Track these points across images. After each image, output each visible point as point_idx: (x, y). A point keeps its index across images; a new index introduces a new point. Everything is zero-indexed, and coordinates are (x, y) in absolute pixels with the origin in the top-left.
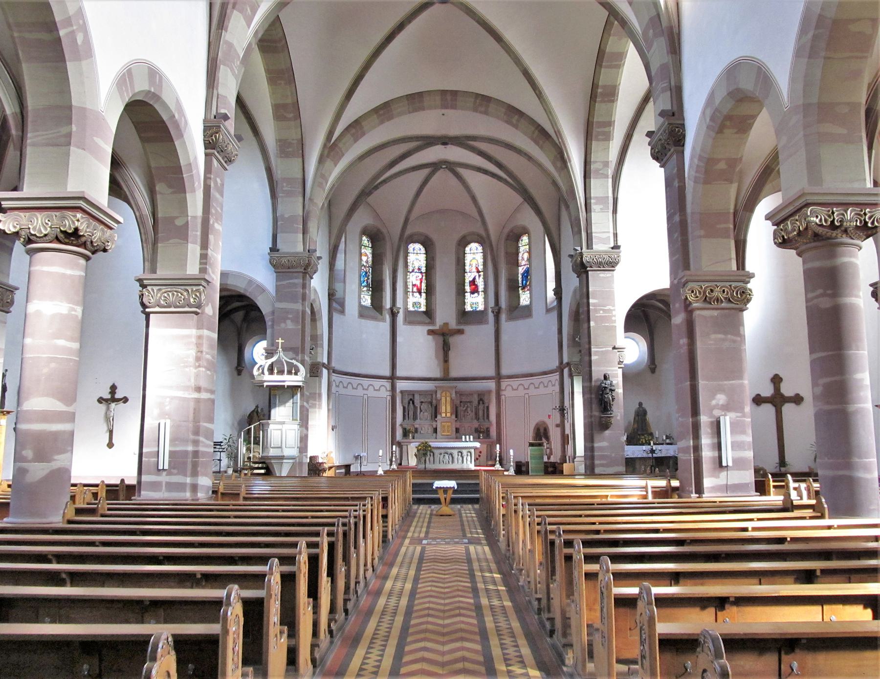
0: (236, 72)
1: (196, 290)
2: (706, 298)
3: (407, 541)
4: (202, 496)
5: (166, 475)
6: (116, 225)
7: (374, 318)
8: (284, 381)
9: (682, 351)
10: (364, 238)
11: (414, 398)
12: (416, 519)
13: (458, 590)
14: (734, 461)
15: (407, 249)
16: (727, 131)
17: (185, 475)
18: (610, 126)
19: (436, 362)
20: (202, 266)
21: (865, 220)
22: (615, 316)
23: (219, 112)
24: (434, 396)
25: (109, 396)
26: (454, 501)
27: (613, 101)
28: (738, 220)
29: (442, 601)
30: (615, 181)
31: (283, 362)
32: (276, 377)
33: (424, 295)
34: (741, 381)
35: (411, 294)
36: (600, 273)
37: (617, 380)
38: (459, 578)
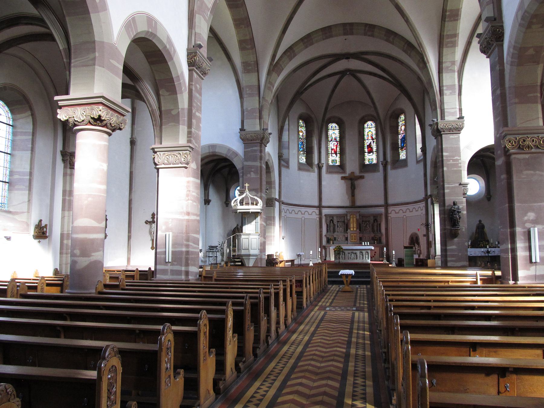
1: (185, 153)
2: (519, 146)
3: (317, 308)
5: (171, 265)
6: (127, 114)
7: (308, 171)
8: (249, 209)
9: (503, 183)
10: (301, 121)
11: (333, 218)
12: (327, 294)
15: (328, 127)
16: (534, 27)
17: (181, 266)
18: (456, 37)
19: (347, 197)
22: (461, 163)
24: (346, 217)
25: (151, 220)
26: (352, 283)
27: (457, 20)
30: (460, 75)
31: (248, 198)
32: (244, 207)
33: (338, 155)
36: (450, 136)
37: (463, 205)
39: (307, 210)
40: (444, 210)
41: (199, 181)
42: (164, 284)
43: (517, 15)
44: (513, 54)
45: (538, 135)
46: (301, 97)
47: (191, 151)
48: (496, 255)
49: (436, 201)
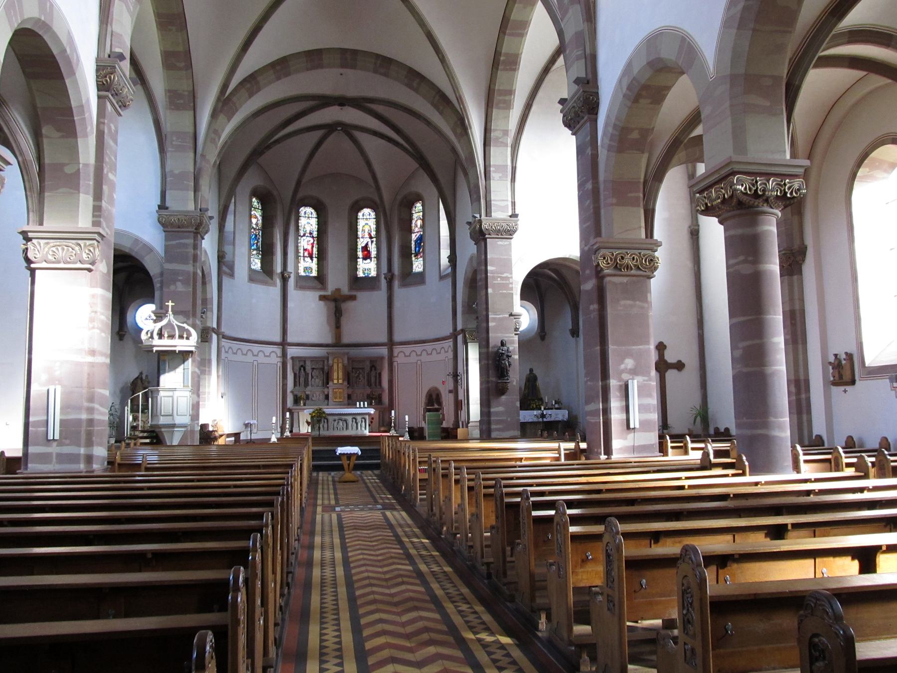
0: (132, 10)
1: (90, 245)
2: (616, 265)
3: (319, 509)
4: (98, 467)
5: (57, 446)
7: (265, 283)
8: (175, 346)
9: (592, 317)
10: (254, 200)
11: (305, 364)
12: (320, 487)
13: (392, 558)
14: (641, 423)
15: (299, 213)
16: (642, 101)
17: (79, 445)
18: (511, 95)
20: (95, 219)
21: (785, 190)
22: (512, 283)
23: (113, 50)
24: (326, 363)
26: (357, 467)
28: (647, 190)
29: (380, 570)
30: (514, 152)
33: (315, 260)
34: (648, 346)
35: (302, 258)
38: (388, 545)
39: (424, 348)
40: (488, 353)
41: (110, 295)
42: (43, 480)
43: (620, 81)
44: (612, 135)
45: (640, 251)
46: (258, 161)
47: (100, 240)
48: (552, 420)
49: (470, 339)
